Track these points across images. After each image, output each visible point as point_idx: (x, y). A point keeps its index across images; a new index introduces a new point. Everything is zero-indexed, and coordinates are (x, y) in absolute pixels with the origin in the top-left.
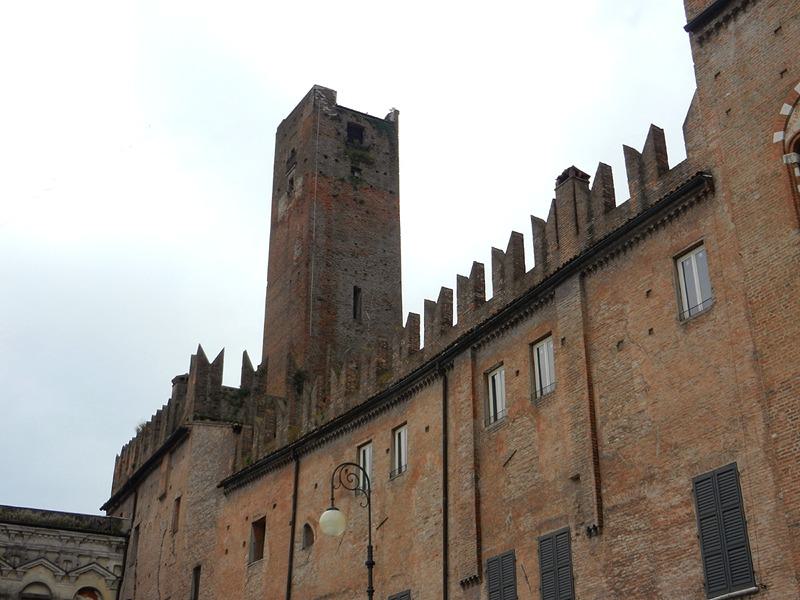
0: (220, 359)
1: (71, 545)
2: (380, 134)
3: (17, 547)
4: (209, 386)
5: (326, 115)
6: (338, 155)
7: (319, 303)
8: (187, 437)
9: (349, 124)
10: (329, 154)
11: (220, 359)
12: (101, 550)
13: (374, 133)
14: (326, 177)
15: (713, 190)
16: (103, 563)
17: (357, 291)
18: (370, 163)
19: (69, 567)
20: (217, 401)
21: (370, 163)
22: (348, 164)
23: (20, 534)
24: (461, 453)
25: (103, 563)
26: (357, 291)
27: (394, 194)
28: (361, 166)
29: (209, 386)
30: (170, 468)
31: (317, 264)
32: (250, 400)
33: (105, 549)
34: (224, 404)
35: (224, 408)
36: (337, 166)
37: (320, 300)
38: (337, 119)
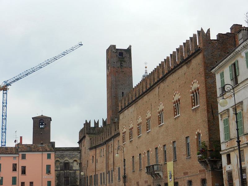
0: (90, 122)
1: (71, 153)
2: (127, 53)
3: (62, 154)
4: (88, 127)
5: (114, 52)
6: (117, 61)
7: (114, 97)
8: (85, 137)
9: (119, 52)
10: (115, 62)
11: (90, 122)
12: (76, 153)
13: (125, 53)
14: (114, 68)
15: (120, 135)
16: (77, 155)
17: (123, 93)
18: (124, 61)
19: (71, 157)
20: (90, 130)
21: (124, 61)
22: (119, 63)
23: (62, 152)
24: (107, 157)
25: (77, 155)
26: (123, 93)
27: (131, 68)
28: (123, 62)
29: (88, 127)
30: (84, 141)
31: (113, 89)
32: (96, 129)
33: (77, 153)
34: (91, 130)
35: (91, 131)
36: (119, 59)
37: (115, 97)
38: (116, 52)
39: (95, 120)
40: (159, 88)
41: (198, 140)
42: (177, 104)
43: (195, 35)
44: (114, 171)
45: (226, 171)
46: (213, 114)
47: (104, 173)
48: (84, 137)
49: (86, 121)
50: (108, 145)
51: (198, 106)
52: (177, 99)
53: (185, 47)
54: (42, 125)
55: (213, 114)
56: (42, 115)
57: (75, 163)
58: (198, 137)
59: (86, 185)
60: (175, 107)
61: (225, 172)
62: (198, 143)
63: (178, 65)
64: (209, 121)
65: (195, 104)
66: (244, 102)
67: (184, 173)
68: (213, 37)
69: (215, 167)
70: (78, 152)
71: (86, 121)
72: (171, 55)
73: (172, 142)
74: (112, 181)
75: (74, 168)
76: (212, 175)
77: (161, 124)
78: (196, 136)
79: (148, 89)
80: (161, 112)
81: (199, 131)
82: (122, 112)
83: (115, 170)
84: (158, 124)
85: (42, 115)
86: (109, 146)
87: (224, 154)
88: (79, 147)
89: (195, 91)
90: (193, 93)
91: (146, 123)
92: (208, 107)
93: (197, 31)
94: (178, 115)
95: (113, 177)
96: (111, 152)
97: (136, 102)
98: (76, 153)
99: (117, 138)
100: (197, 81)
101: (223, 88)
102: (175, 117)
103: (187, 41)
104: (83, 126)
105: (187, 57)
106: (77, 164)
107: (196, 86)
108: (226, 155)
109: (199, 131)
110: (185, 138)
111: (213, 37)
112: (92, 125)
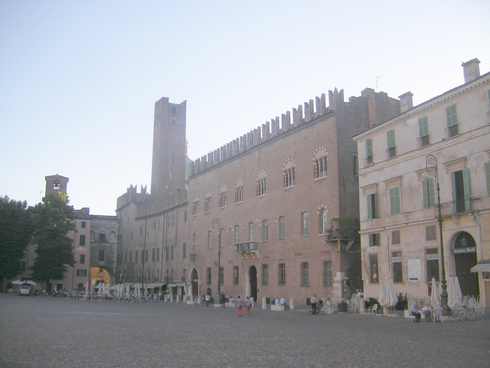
33: (116, 223)
39: (146, 185)
40: (284, 140)
41: (321, 216)
42: (288, 173)
43: (259, 128)
44: (176, 247)
45: (366, 254)
46: (344, 186)
47: (158, 249)
48: (128, 204)
49: (131, 186)
50: (167, 216)
51: (241, 202)
52: (291, 168)
53: (256, 134)
54: (57, 186)
55: (344, 186)
56: (57, 175)
57: (113, 235)
58: (321, 214)
59: (489, 211)
60: (286, 176)
61: (364, 255)
62: (321, 220)
63: (221, 163)
64: (340, 195)
65: (238, 199)
66: (404, 176)
67: (321, 252)
68: (346, 100)
69: (344, 248)
70: (116, 222)
71: (131, 186)
72: (241, 137)
73: (277, 217)
74: (172, 258)
75: (111, 241)
76: (341, 257)
77: (238, 203)
78: (228, 231)
79: (207, 168)
80: (224, 194)
81: (231, 226)
82: (194, 178)
83: (177, 246)
84: (235, 202)
85: (57, 175)
86: (169, 217)
87: (363, 234)
88: (116, 215)
89: (240, 188)
90: (286, 172)
91: (235, 193)
92: (339, 179)
93: (293, 108)
94: (240, 202)
95: (175, 254)
96: (173, 224)
97: (219, 167)
98: (114, 223)
99: (184, 209)
100: (324, 149)
101: (370, 158)
102: (284, 189)
103: (224, 145)
104: (126, 191)
105: (217, 164)
106: (115, 236)
107: (321, 154)
108: (368, 235)
109: (231, 226)
110: (300, 214)
111: (346, 100)
112: (139, 191)
